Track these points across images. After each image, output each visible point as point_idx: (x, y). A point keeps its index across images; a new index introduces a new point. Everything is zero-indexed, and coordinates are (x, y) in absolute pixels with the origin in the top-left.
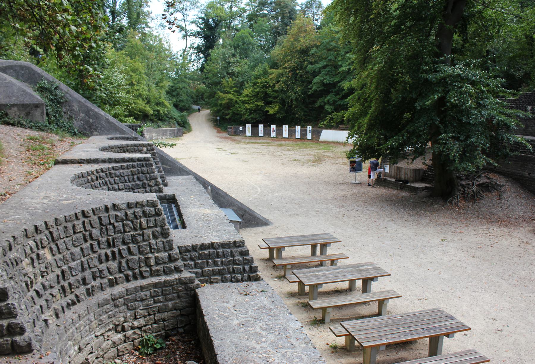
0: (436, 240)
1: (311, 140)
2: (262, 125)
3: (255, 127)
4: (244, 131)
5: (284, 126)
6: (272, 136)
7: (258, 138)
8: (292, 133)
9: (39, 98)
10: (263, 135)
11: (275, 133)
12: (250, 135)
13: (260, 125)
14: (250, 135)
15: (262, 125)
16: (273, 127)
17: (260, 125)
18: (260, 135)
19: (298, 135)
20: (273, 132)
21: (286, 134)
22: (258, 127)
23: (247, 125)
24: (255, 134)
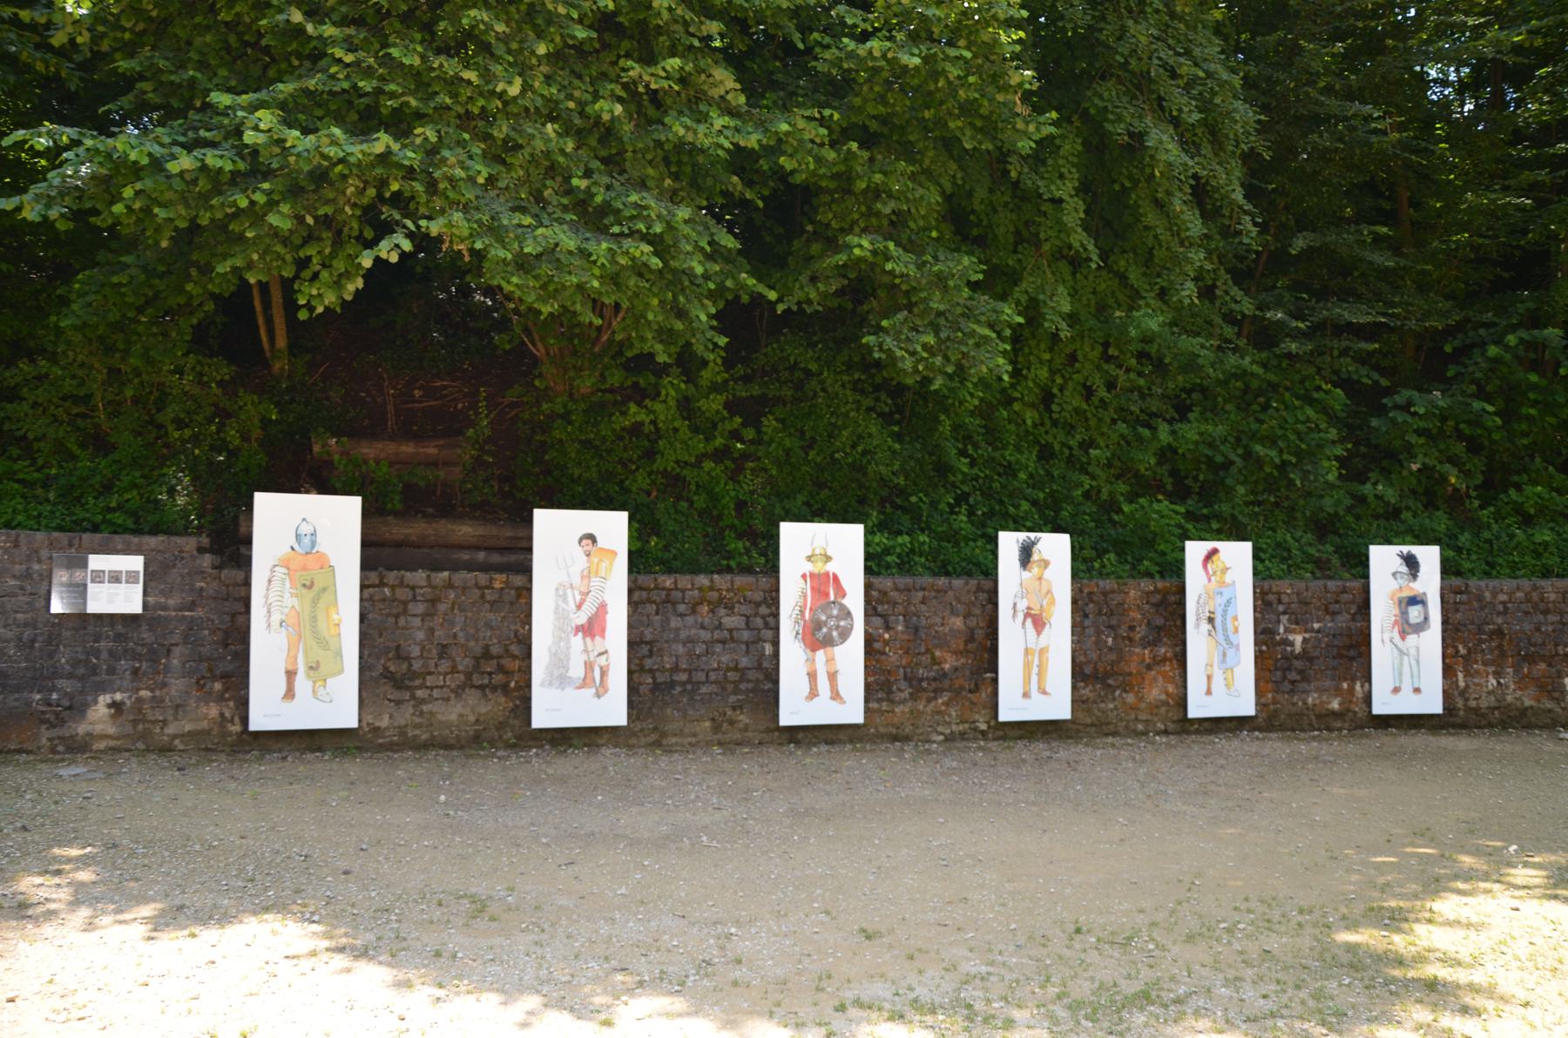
0: (23, 946)
1: (1456, 718)
2: (613, 527)
3: (701, 555)
4: (209, 635)
5: (1195, 551)
6: (794, 710)
7: (758, 774)
8: (1130, 637)
9: (1342, 791)
10: (612, 710)
11: (851, 656)
12: (336, 703)
13: (557, 532)
14: (336, 703)
15: (613, 527)
16: (822, 555)
17: (557, 532)
18: (551, 708)
19: (1221, 673)
20: (818, 637)
21: (1035, 660)
22: (516, 559)
23: (276, 517)
24: (446, 680)
